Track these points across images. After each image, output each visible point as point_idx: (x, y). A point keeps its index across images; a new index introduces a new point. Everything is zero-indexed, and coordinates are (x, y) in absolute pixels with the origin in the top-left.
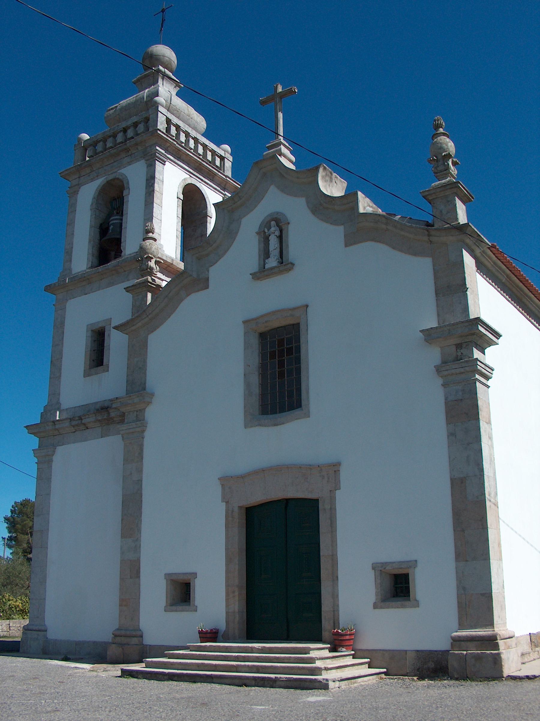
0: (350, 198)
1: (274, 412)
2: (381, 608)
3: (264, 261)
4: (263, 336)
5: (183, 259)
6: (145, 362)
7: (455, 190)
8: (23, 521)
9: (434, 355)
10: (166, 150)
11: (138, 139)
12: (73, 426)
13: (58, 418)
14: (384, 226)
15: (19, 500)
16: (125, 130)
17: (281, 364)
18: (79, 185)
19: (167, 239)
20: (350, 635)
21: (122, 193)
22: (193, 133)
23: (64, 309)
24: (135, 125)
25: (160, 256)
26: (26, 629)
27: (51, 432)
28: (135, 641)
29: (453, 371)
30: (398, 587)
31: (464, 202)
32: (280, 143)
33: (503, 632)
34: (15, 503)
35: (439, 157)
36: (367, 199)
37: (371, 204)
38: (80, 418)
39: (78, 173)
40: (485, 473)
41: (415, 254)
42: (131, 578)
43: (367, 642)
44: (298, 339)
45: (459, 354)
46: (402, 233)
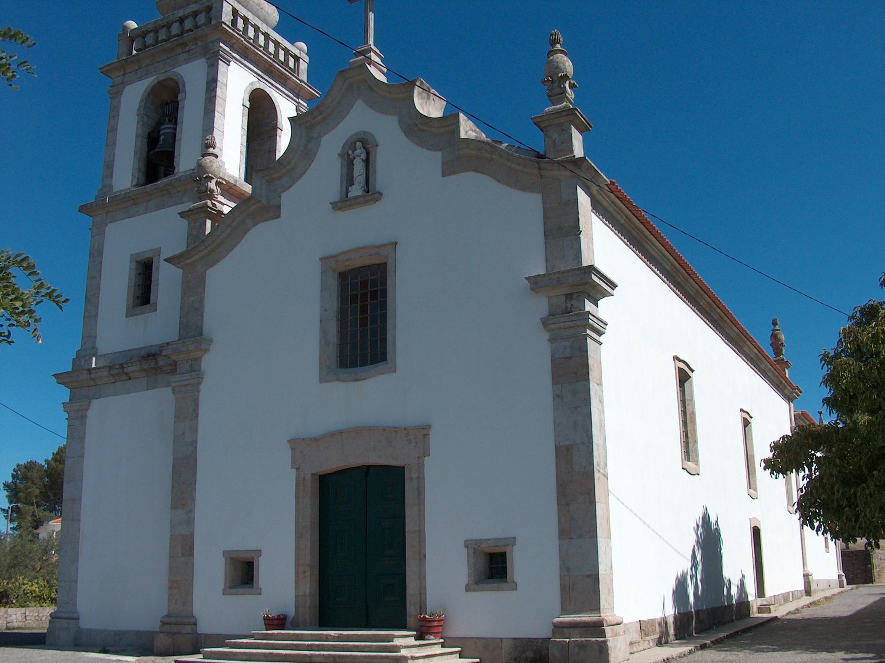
0: (450, 121)
1: (354, 365)
2: (475, 590)
3: (347, 189)
4: (343, 276)
5: (248, 179)
6: (202, 301)
7: (571, 118)
8: (27, 488)
9: (540, 306)
10: (231, 48)
11: (198, 32)
12: (113, 376)
13: (93, 366)
14: (488, 156)
15: (23, 462)
16: (181, 20)
17: (364, 310)
18: (124, 84)
19: (230, 157)
20: (439, 621)
21: (177, 97)
22: (264, 28)
23: (102, 234)
24: (195, 14)
25: (221, 175)
26: (54, 617)
27: (83, 383)
28: (188, 629)
29: (562, 325)
30: (494, 567)
31: (581, 132)
32: (371, 50)
33: (611, 618)
34: (18, 465)
35: (555, 78)
36: (470, 122)
37: (474, 128)
38: (122, 366)
39: (122, 70)
40: (594, 440)
41: (523, 189)
42: (183, 555)
43: (459, 628)
44: (384, 281)
45: (569, 305)
46: (509, 164)
